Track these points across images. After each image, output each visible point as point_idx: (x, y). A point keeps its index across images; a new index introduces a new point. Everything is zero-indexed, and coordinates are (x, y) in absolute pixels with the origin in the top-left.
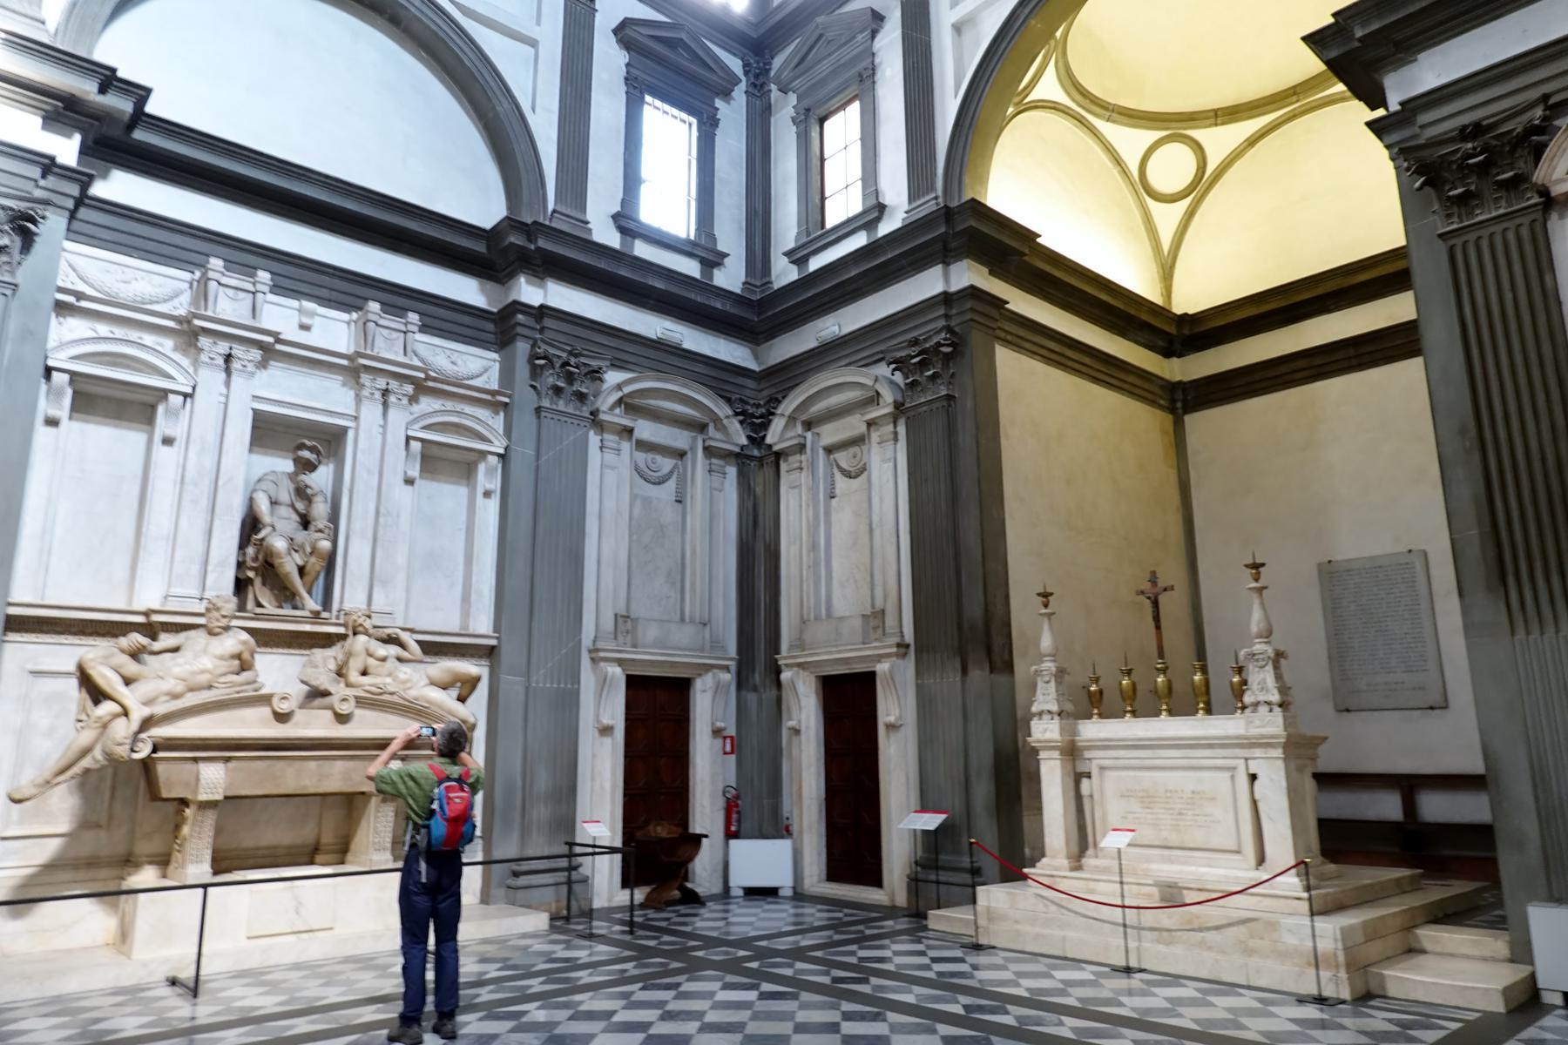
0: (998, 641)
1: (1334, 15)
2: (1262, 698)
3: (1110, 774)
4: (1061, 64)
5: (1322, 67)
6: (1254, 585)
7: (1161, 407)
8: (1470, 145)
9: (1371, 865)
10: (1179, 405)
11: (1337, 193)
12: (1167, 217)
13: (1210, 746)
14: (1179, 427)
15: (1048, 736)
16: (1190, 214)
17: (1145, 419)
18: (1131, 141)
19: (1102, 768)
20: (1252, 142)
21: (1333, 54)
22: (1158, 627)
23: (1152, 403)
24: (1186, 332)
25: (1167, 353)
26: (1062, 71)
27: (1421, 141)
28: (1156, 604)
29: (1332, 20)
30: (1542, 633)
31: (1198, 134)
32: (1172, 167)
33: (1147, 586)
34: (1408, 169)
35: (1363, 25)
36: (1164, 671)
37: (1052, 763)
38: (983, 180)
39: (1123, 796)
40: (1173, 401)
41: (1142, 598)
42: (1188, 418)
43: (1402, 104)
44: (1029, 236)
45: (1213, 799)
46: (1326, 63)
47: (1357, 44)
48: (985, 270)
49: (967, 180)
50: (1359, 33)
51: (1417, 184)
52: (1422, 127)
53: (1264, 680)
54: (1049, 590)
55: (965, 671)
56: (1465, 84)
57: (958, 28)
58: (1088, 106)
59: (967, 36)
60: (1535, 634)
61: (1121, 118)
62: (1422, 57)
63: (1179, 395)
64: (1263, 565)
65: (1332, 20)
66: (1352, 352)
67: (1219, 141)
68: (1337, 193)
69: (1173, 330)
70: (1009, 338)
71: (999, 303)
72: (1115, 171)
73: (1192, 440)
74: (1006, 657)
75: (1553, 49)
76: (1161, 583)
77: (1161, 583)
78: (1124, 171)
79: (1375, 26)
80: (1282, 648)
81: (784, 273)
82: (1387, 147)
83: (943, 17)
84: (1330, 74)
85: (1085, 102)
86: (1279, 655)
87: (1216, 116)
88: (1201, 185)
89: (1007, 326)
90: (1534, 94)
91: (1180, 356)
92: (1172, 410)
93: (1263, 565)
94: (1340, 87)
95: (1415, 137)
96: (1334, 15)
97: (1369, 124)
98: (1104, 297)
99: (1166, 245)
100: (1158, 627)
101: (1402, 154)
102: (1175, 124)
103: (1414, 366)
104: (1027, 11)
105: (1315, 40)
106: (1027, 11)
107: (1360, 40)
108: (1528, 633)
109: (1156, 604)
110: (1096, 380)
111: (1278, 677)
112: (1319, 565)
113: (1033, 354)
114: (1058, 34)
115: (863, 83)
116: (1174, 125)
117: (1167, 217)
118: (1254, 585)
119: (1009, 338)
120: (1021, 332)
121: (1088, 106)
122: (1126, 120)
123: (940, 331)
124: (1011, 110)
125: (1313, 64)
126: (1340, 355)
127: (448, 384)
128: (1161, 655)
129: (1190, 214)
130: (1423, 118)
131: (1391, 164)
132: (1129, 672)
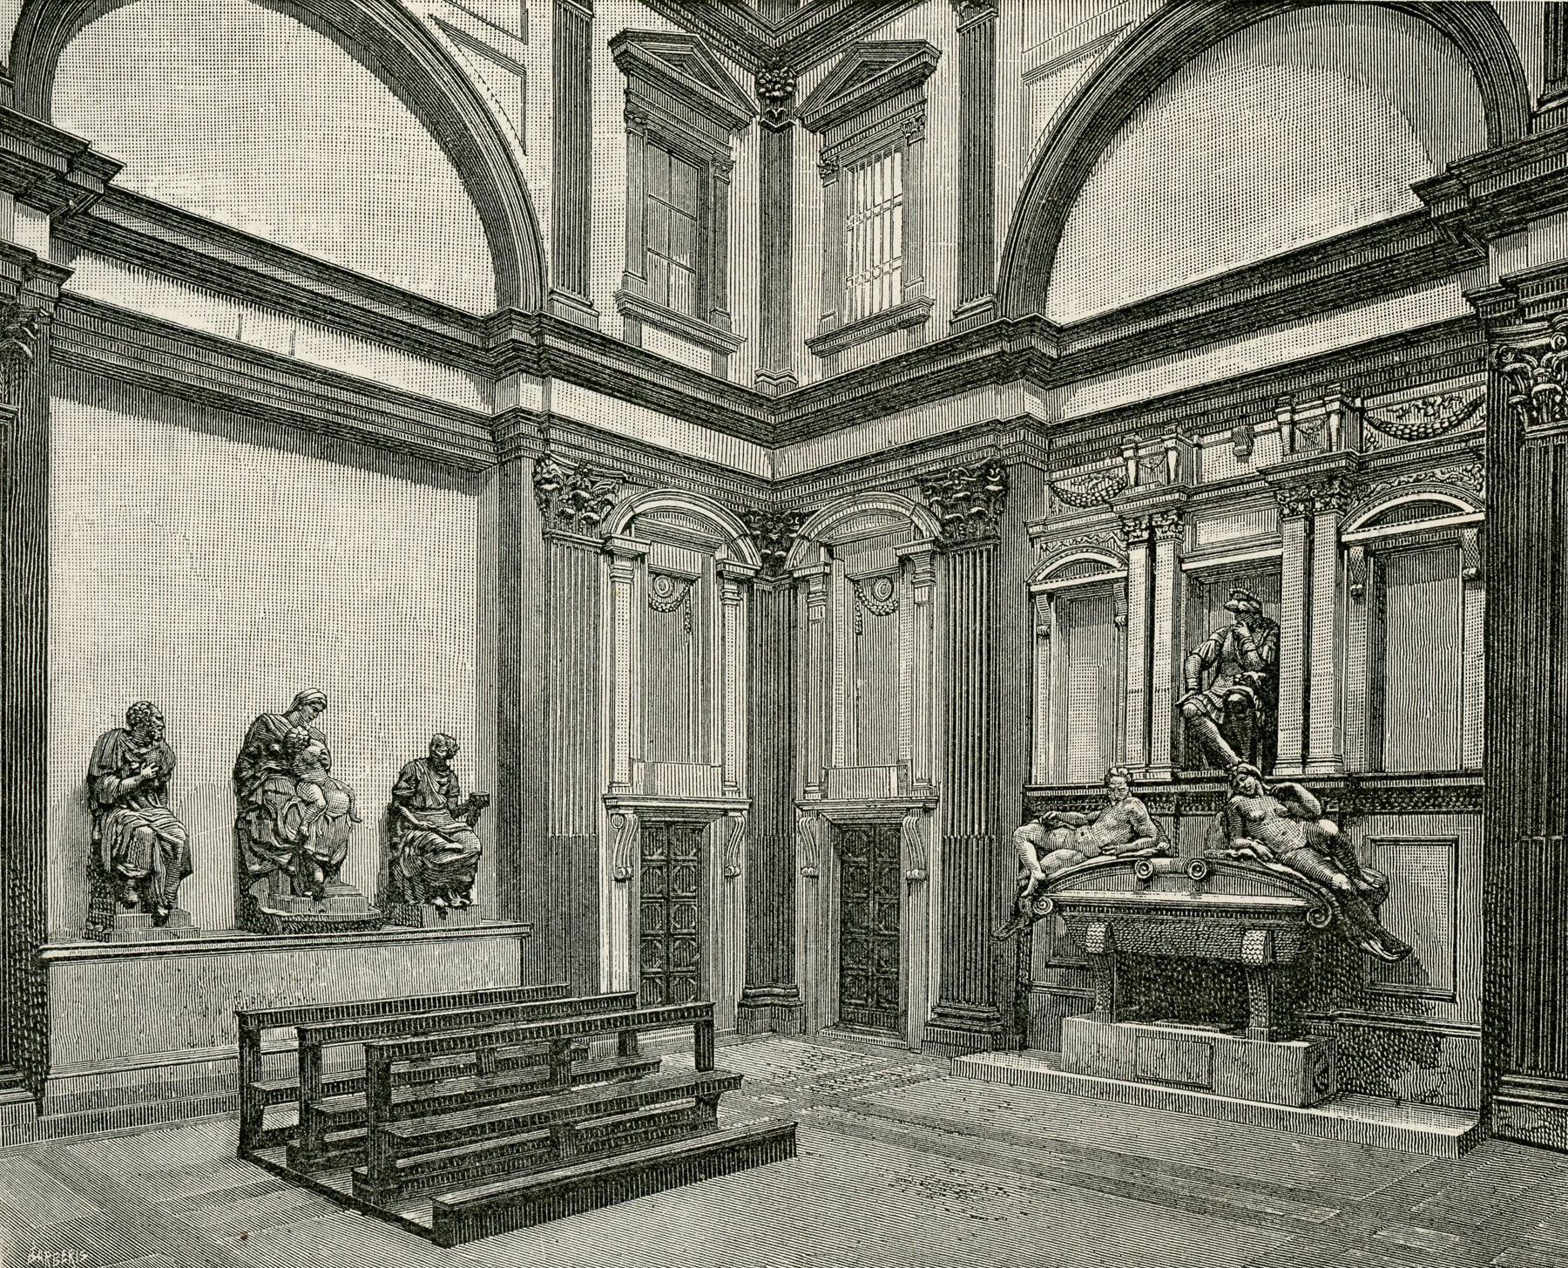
81: (809, 371)
115: (913, 130)
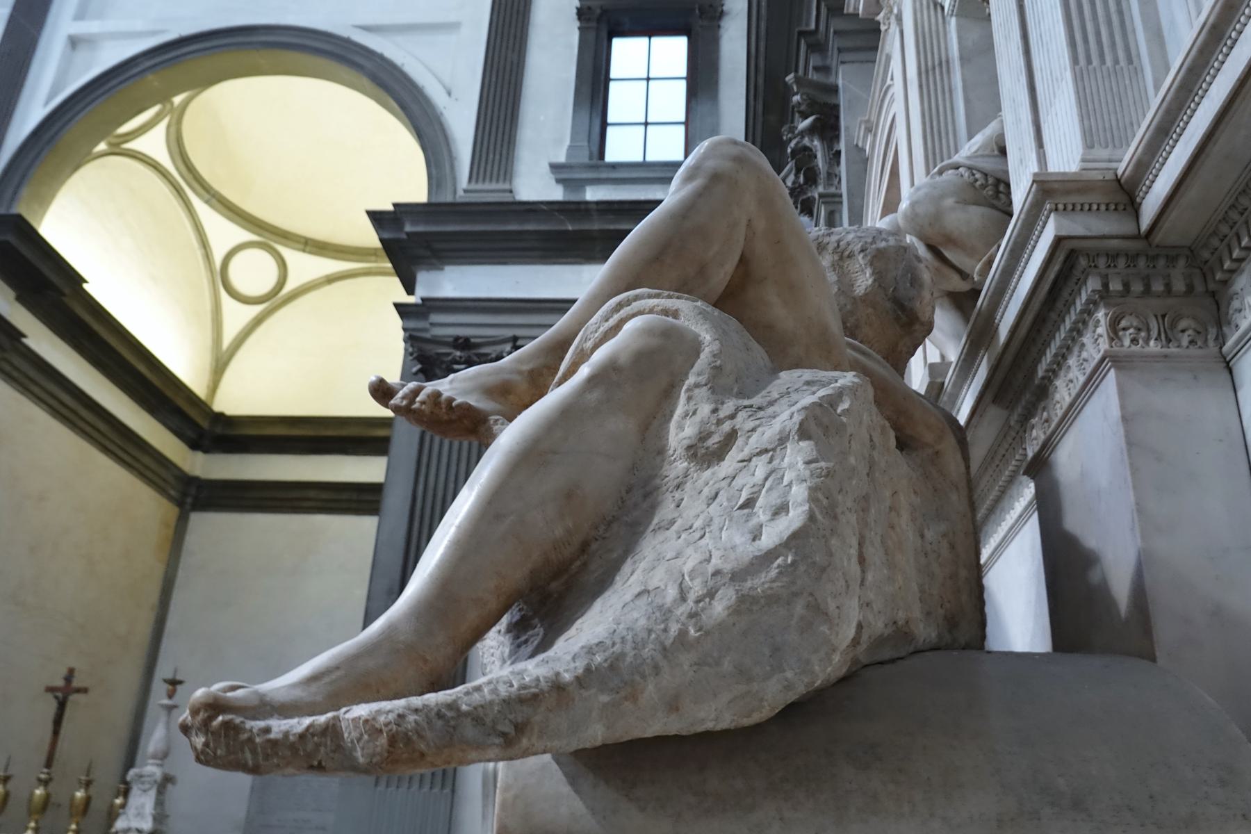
1: (395, 205)
4: (173, 129)
5: (378, 244)
6: (166, 701)
7: (170, 498)
8: (458, 353)
10: (189, 500)
11: (331, 351)
12: (236, 316)
14: (182, 521)
16: (258, 322)
17: (148, 505)
18: (224, 233)
20: (331, 279)
21: (386, 236)
22: (56, 733)
23: (161, 490)
24: (219, 430)
25: (194, 445)
26: (173, 137)
27: (427, 335)
28: (62, 705)
29: (391, 208)
30: (409, 788)
31: (288, 254)
32: (253, 272)
33: (60, 683)
34: (411, 354)
35: (414, 223)
36: (45, 783)
38: (44, 202)
40: (185, 495)
41: (50, 696)
43: (423, 300)
44: (76, 280)
46: (381, 240)
47: (405, 236)
48: (11, 294)
49: (25, 192)
50: (408, 228)
51: (414, 370)
52: (431, 324)
53: (143, 806)
54: (178, 678)
56: (469, 304)
57: (74, 42)
58: (187, 179)
59: (81, 55)
60: (392, 789)
62: (448, 269)
63: (193, 491)
64: (180, 682)
65: (391, 208)
66: (354, 496)
67: (304, 267)
68: (331, 351)
69: (205, 424)
70: (15, 374)
71: (15, 335)
72: (199, 253)
75: (529, 305)
76: (76, 683)
77: (76, 683)
78: (208, 256)
79: (420, 228)
80: (172, 773)
82: (405, 329)
83: (62, 24)
84: (383, 253)
85: (189, 177)
86: (168, 780)
88: (275, 300)
89: (17, 361)
90: (509, 333)
91: (206, 451)
92: (180, 504)
93: (180, 682)
94: (390, 265)
95: (425, 330)
96: (395, 205)
97: (397, 306)
98: (142, 368)
99: (227, 340)
100: (56, 733)
101: (412, 338)
102: (269, 235)
103: (369, 524)
104: (148, 64)
105: (376, 217)
106: (148, 64)
107: (408, 234)
108: (388, 786)
109: (62, 705)
110: (105, 450)
111: (159, 803)
113: (39, 400)
114: (177, 100)
117: (236, 316)
118: (166, 701)
119: (15, 374)
120: (32, 373)
121: (187, 179)
122: (225, 211)
124: (102, 147)
125: (369, 237)
126: (344, 496)
127: (178, 57)
128: (49, 763)
129: (258, 322)
130: (436, 318)
131: (403, 344)
132: (88, 784)
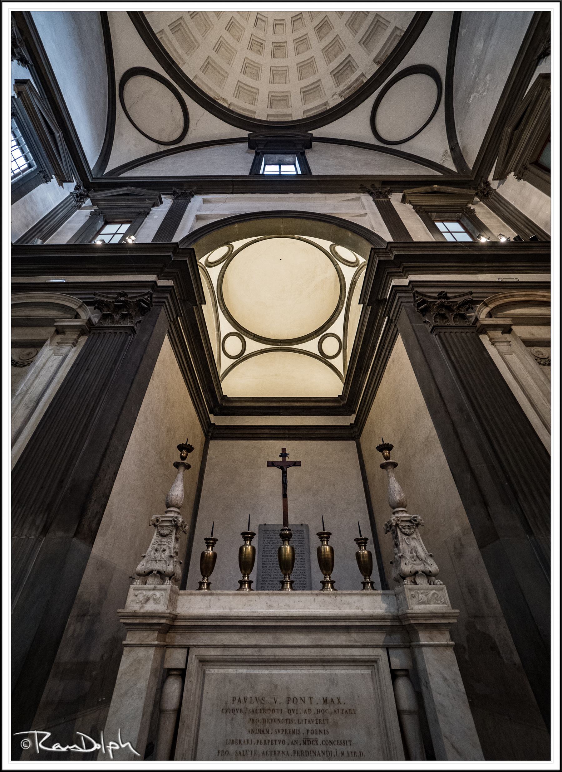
0: (93, 507)
2: (419, 568)
3: (214, 671)
9: (324, 760)
13: (347, 629)
15: (150, 607)
19: (203, 661)
37: (141, 653)
39: (226, 710)
42: (211, 442)
45: (351, 712)
55: (45, 530)
61: (227, 315)
67: (253, 346)
73: (210, 453)
74: (94, 525)
78: (219, 335)
87: (254, 337)
112: (260, 525)
116: (241, 330)
123: (146, 294)
